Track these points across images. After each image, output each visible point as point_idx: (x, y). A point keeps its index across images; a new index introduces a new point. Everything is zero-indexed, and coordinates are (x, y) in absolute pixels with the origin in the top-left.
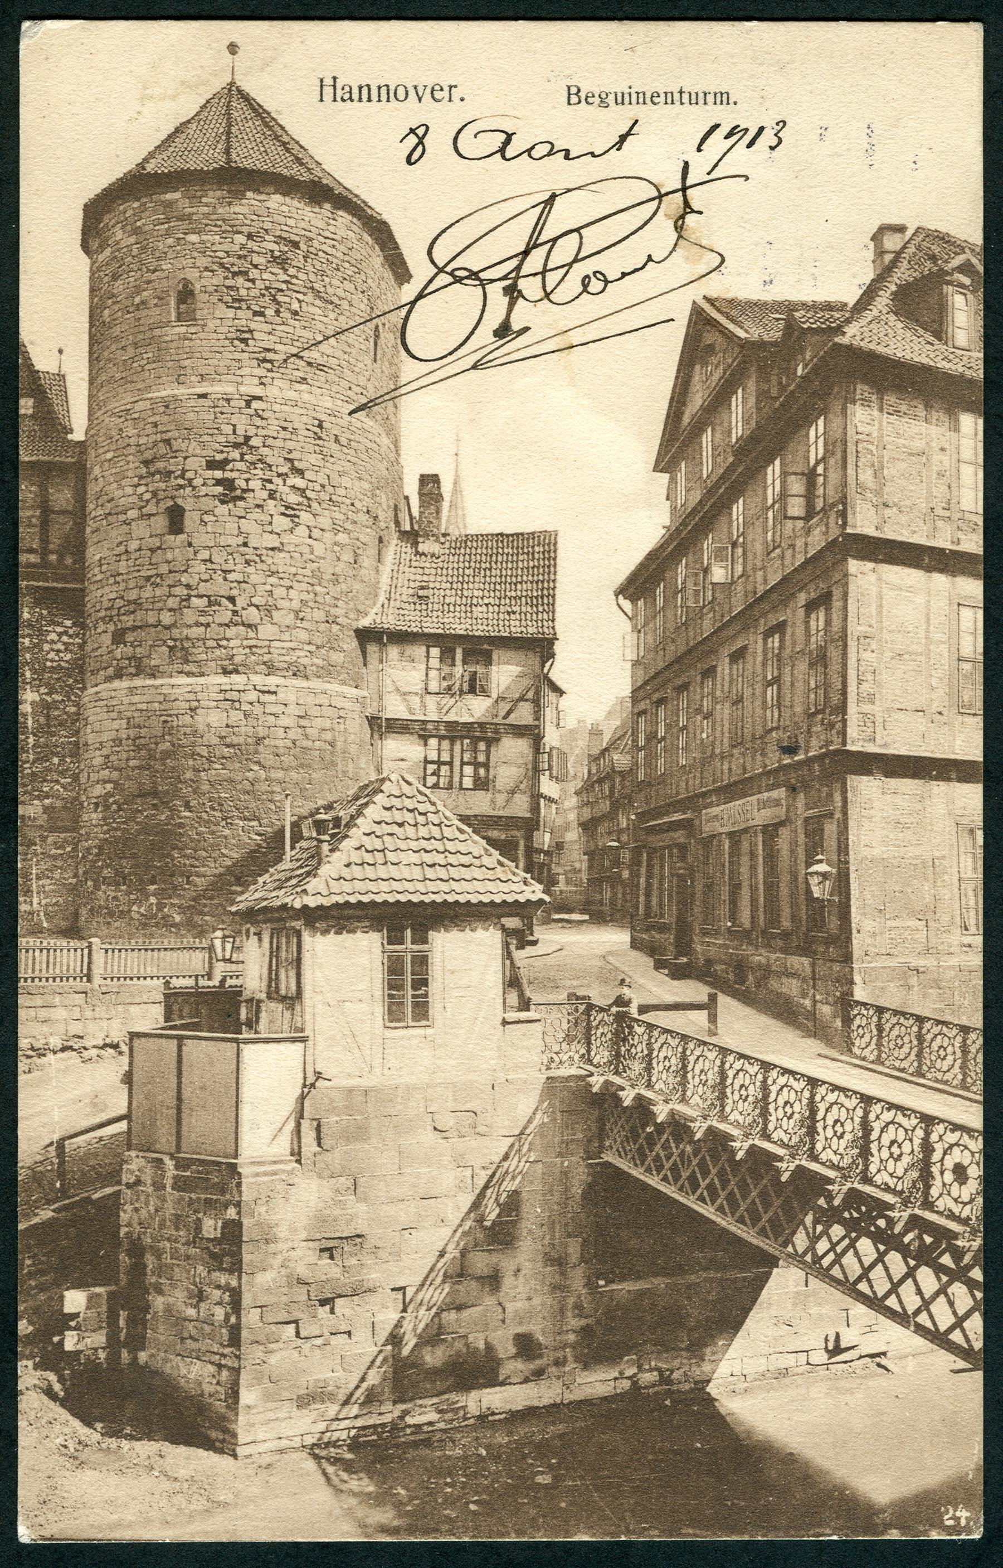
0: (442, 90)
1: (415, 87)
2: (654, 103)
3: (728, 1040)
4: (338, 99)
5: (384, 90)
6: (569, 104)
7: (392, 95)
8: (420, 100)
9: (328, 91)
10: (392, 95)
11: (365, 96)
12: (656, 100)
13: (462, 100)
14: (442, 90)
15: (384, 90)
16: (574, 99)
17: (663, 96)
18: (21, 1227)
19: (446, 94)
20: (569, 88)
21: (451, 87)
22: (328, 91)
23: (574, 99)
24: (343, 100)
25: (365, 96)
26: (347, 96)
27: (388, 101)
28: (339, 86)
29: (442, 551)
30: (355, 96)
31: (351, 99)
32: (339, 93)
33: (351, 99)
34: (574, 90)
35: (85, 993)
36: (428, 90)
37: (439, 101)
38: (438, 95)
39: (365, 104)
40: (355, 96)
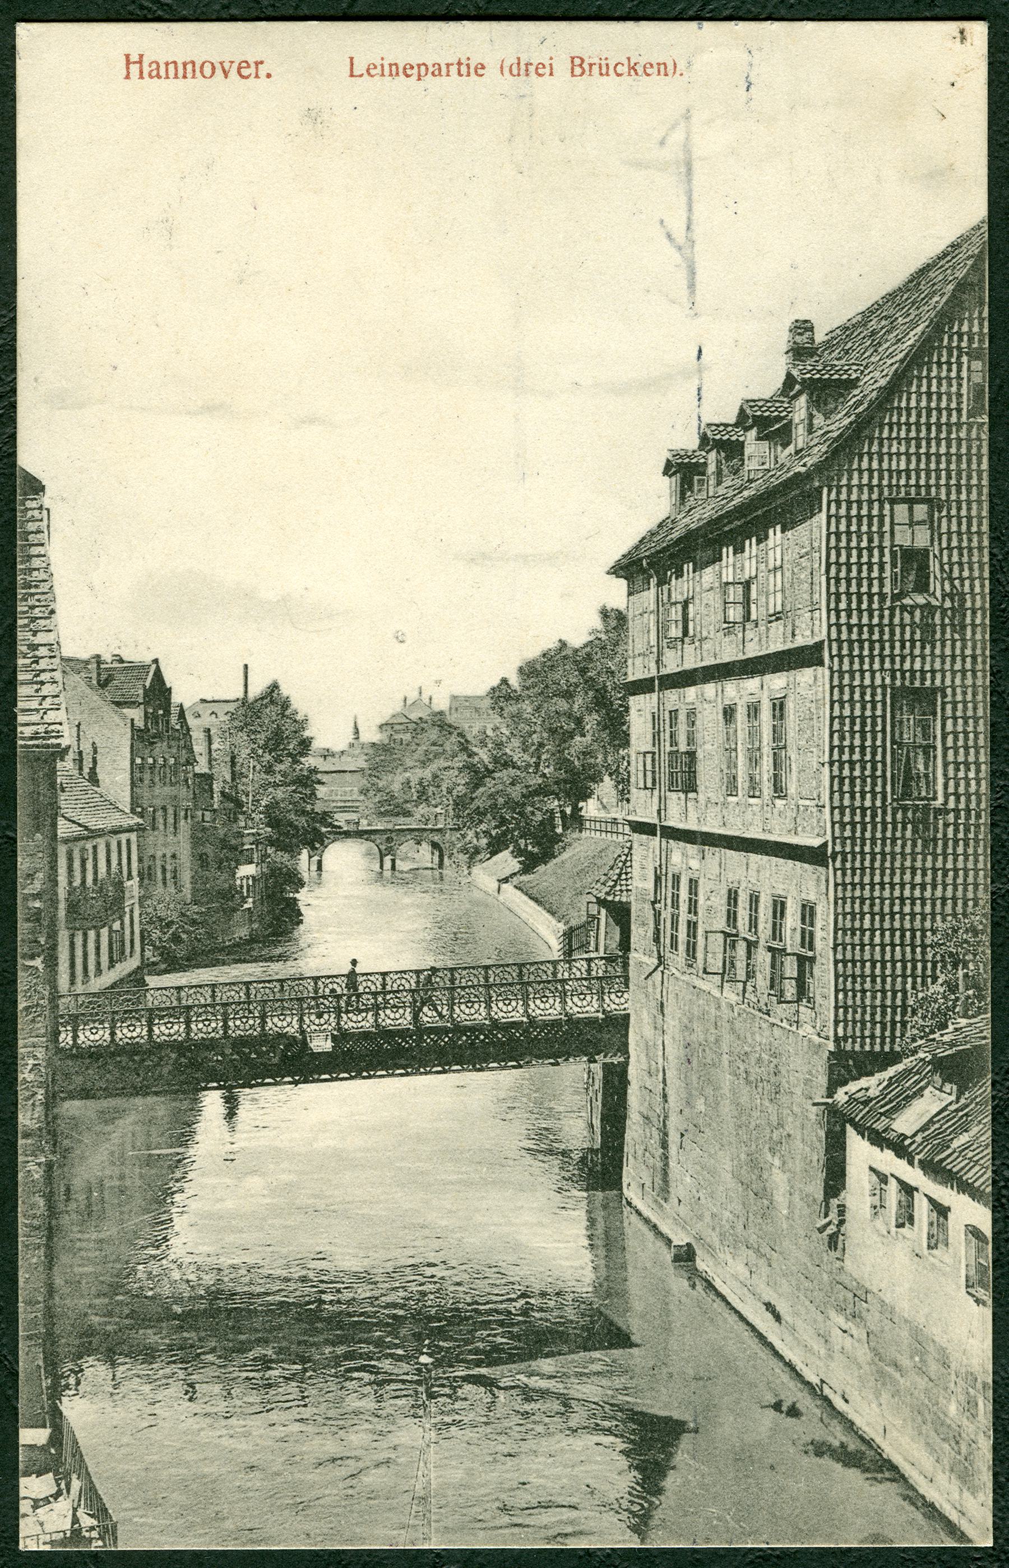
0: (249, 66)
1: (221, 63)
2: (408, 76)
3: (380, 1532)
4: (145, 74)
5: (189, 67)
6: (573, 75)
7: (198, 70)
8: (226, 77)
9: (134, 69)
10: (198, 70)
11: (172, 73)
12: (409, 72)
13: (269, 76)
14: (249, 66)
15: (189, 67)
16: (578, 71)
17: (656, 66)
18: (989, 1015)
19: (252, 70)
20: (573, 58)
21: (257, 64)
22: (134, 69)
23: (578, 71)
24: (151, 76)
25: (172, 73)
26: (154, 73)
27: (194, 77)
28: (145, 65)
29: (57, 690)
30: (163, 73)
31: (159, 76)
32: (146, 70)
33: (159, 76)
34: (577, 61)
35: (705, 972)
36: (235, 66)
37: (247, 77)
38: (372, 72)
39: (172, 81)
40: (163, 73)
